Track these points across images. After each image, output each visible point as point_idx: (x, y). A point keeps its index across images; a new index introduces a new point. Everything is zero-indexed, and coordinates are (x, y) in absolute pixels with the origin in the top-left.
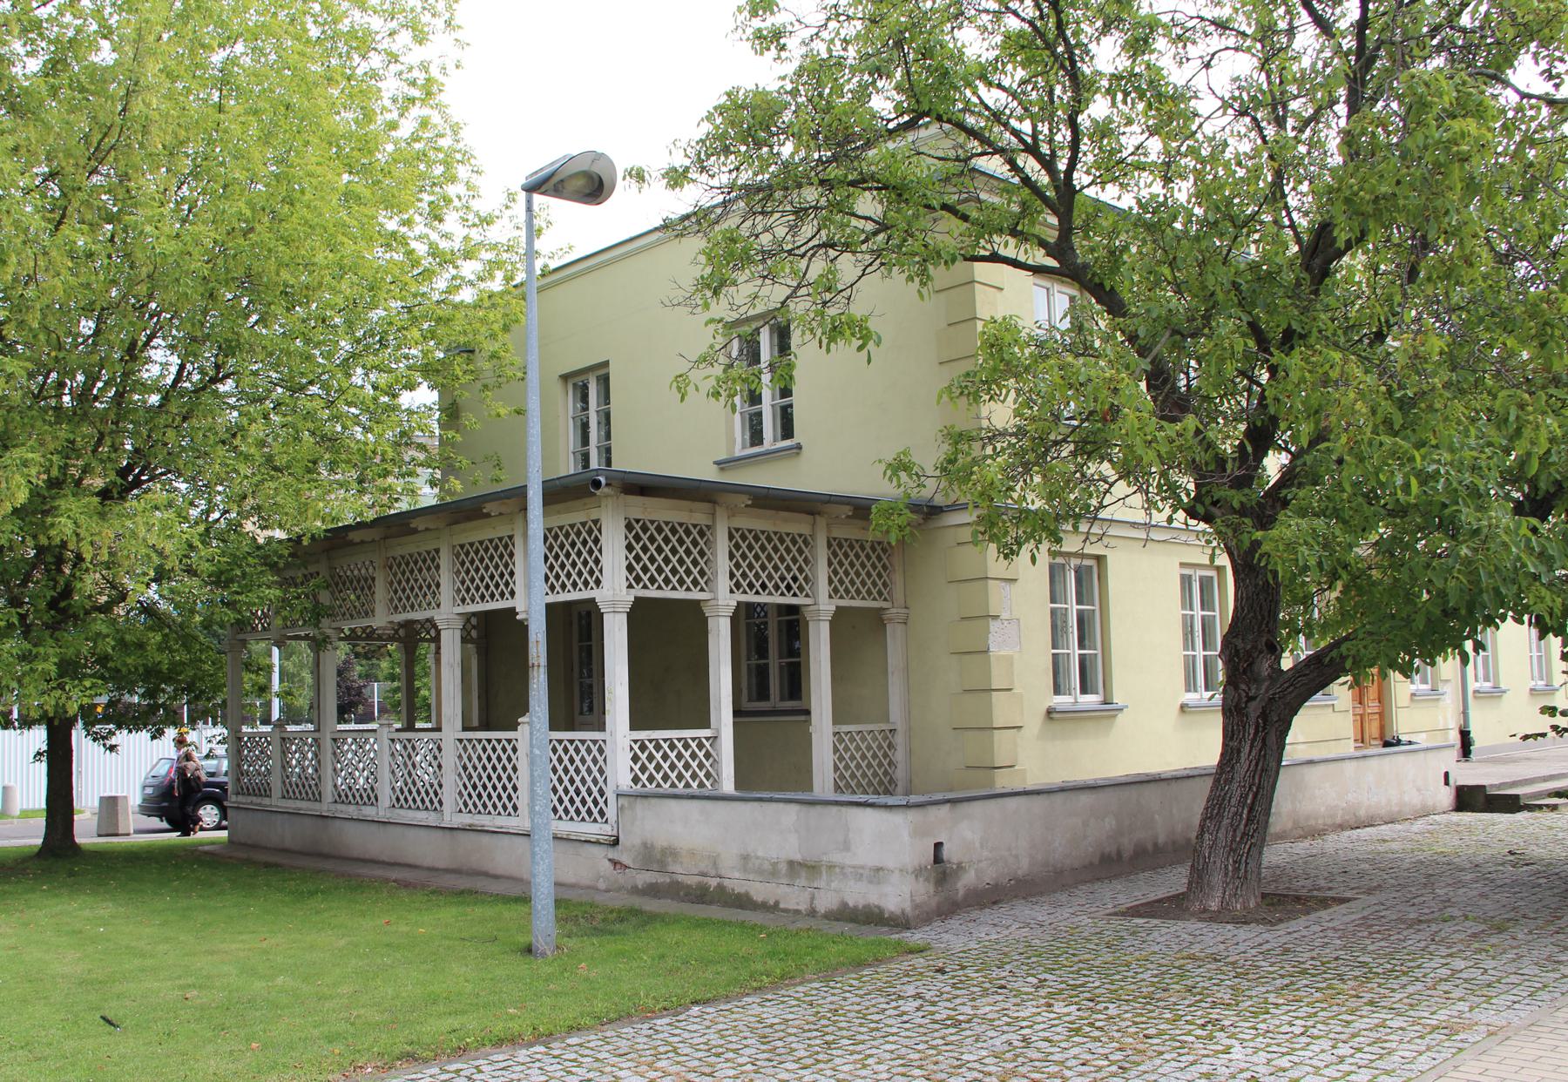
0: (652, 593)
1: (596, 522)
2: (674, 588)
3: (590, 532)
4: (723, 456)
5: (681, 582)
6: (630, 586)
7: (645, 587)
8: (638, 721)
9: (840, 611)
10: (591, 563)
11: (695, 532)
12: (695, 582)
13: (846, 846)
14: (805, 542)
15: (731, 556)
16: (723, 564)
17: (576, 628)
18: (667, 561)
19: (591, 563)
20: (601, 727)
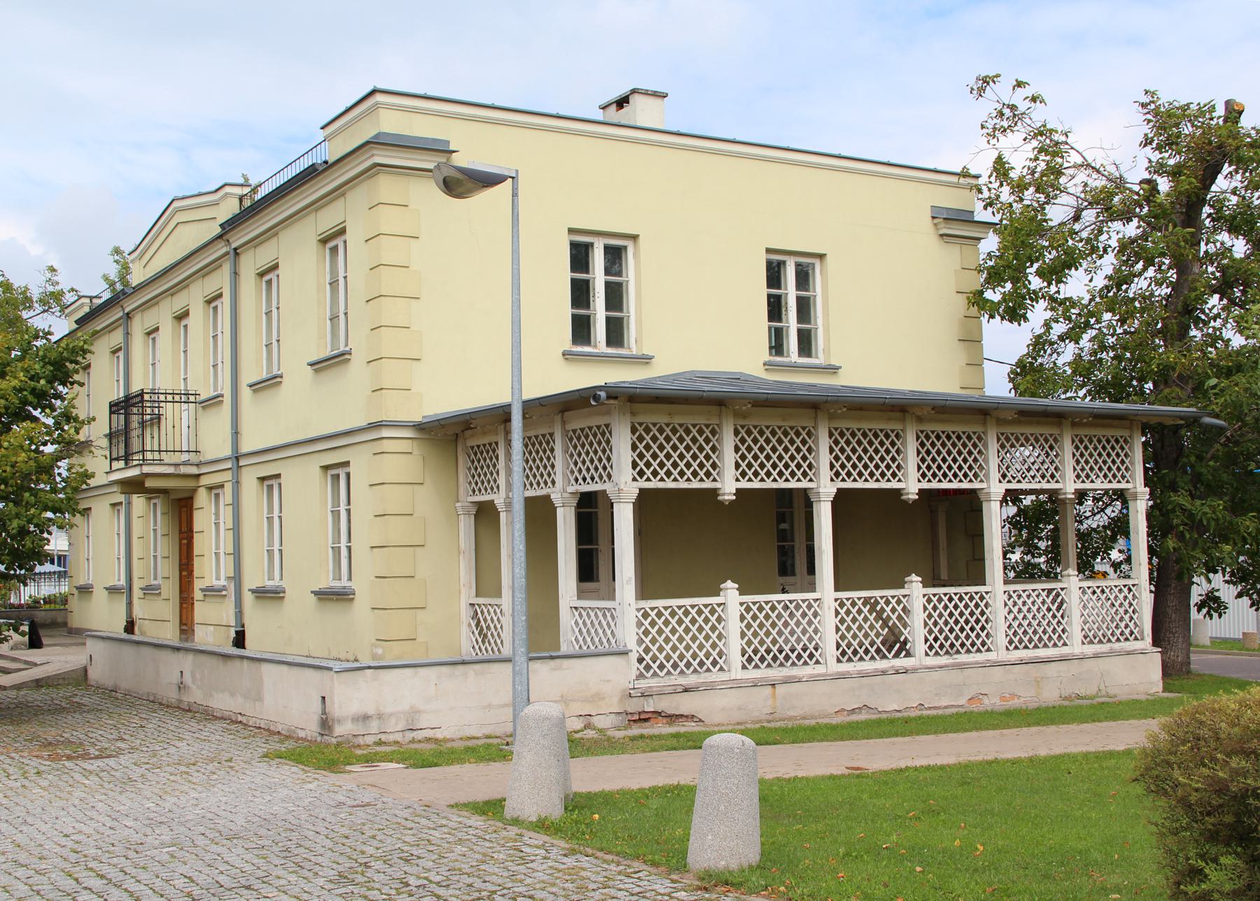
0: (849, 484)
1: (607, 426)
2: (855, 480)
3: (603, 434)
4: (315, 358)
5: (860, 474)
6: (634, 479)
7: (843, 480)
8: (645, 590)
9: (840, 492)
10: (604, 461)
11: (933, 437)
12: (805, 474)
13: (259, 698)
14: (1126, 441)
15: (737, 449)
16: (824, 458)
17: (592, 514)
18: (860, 459)
19: (604, 461)
20: (612, 597)
